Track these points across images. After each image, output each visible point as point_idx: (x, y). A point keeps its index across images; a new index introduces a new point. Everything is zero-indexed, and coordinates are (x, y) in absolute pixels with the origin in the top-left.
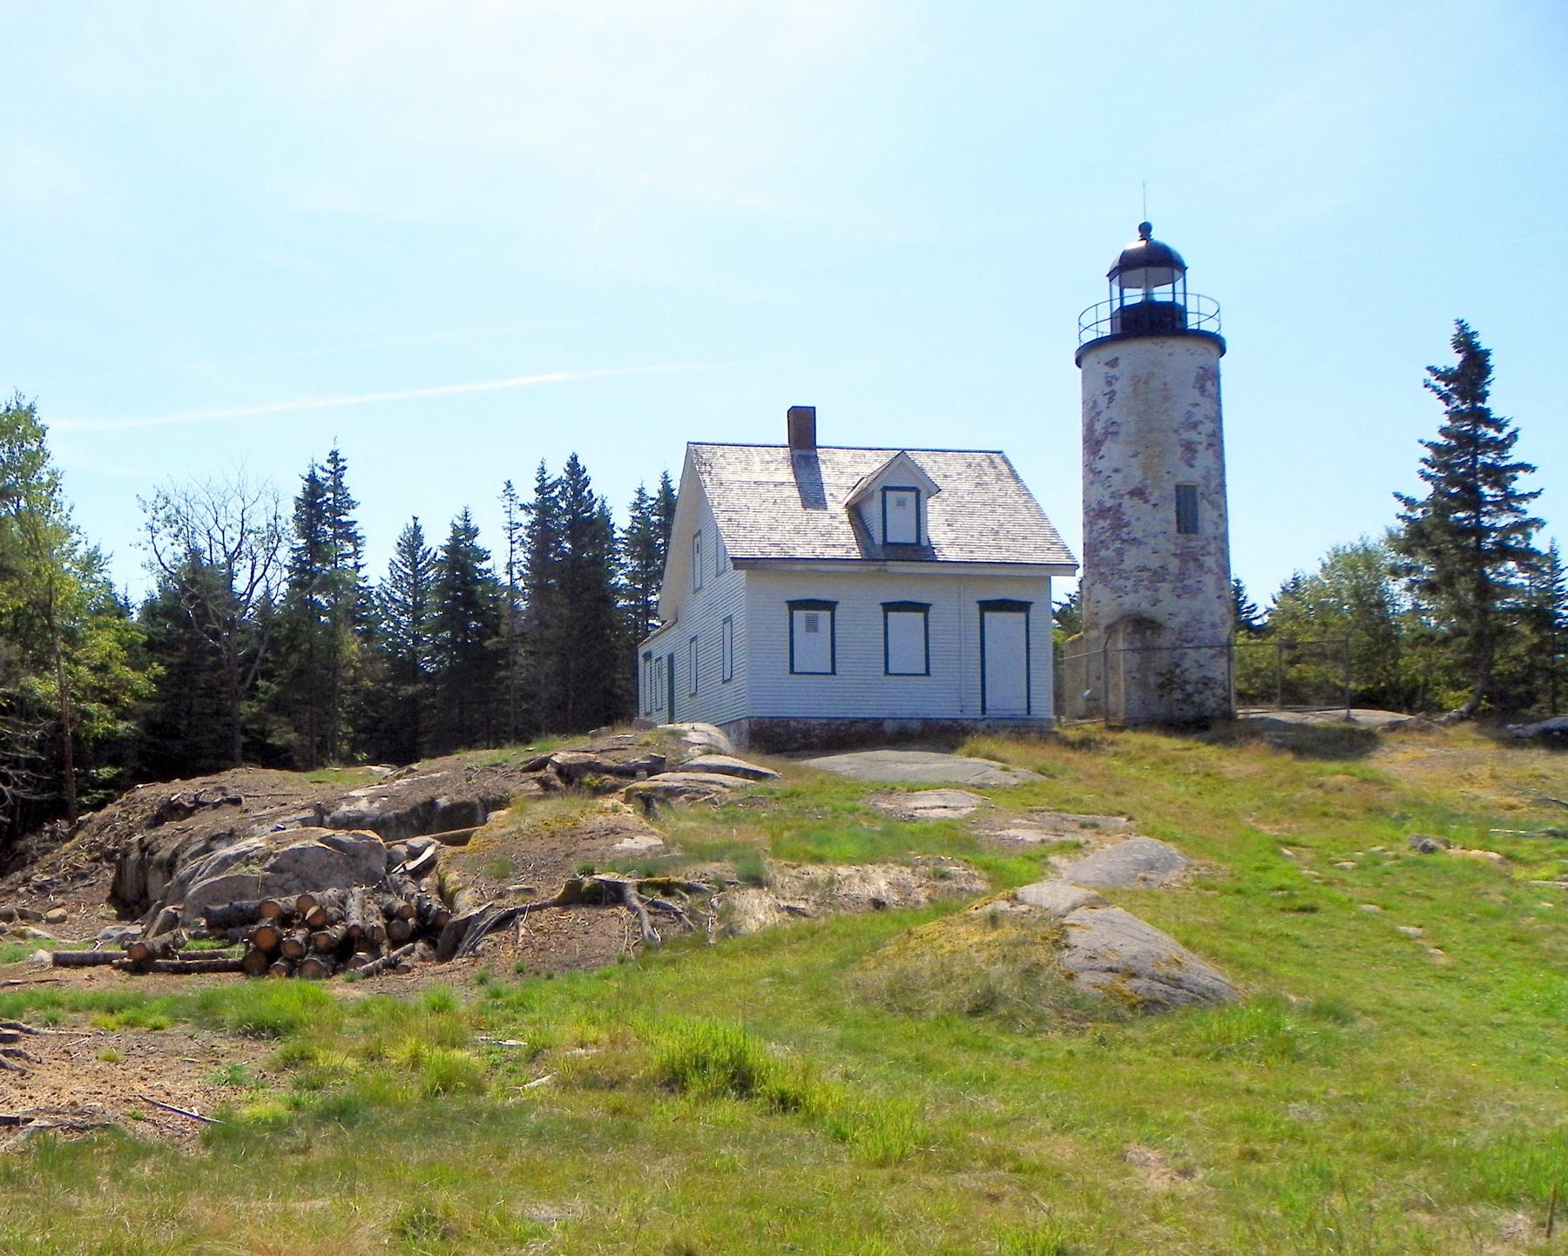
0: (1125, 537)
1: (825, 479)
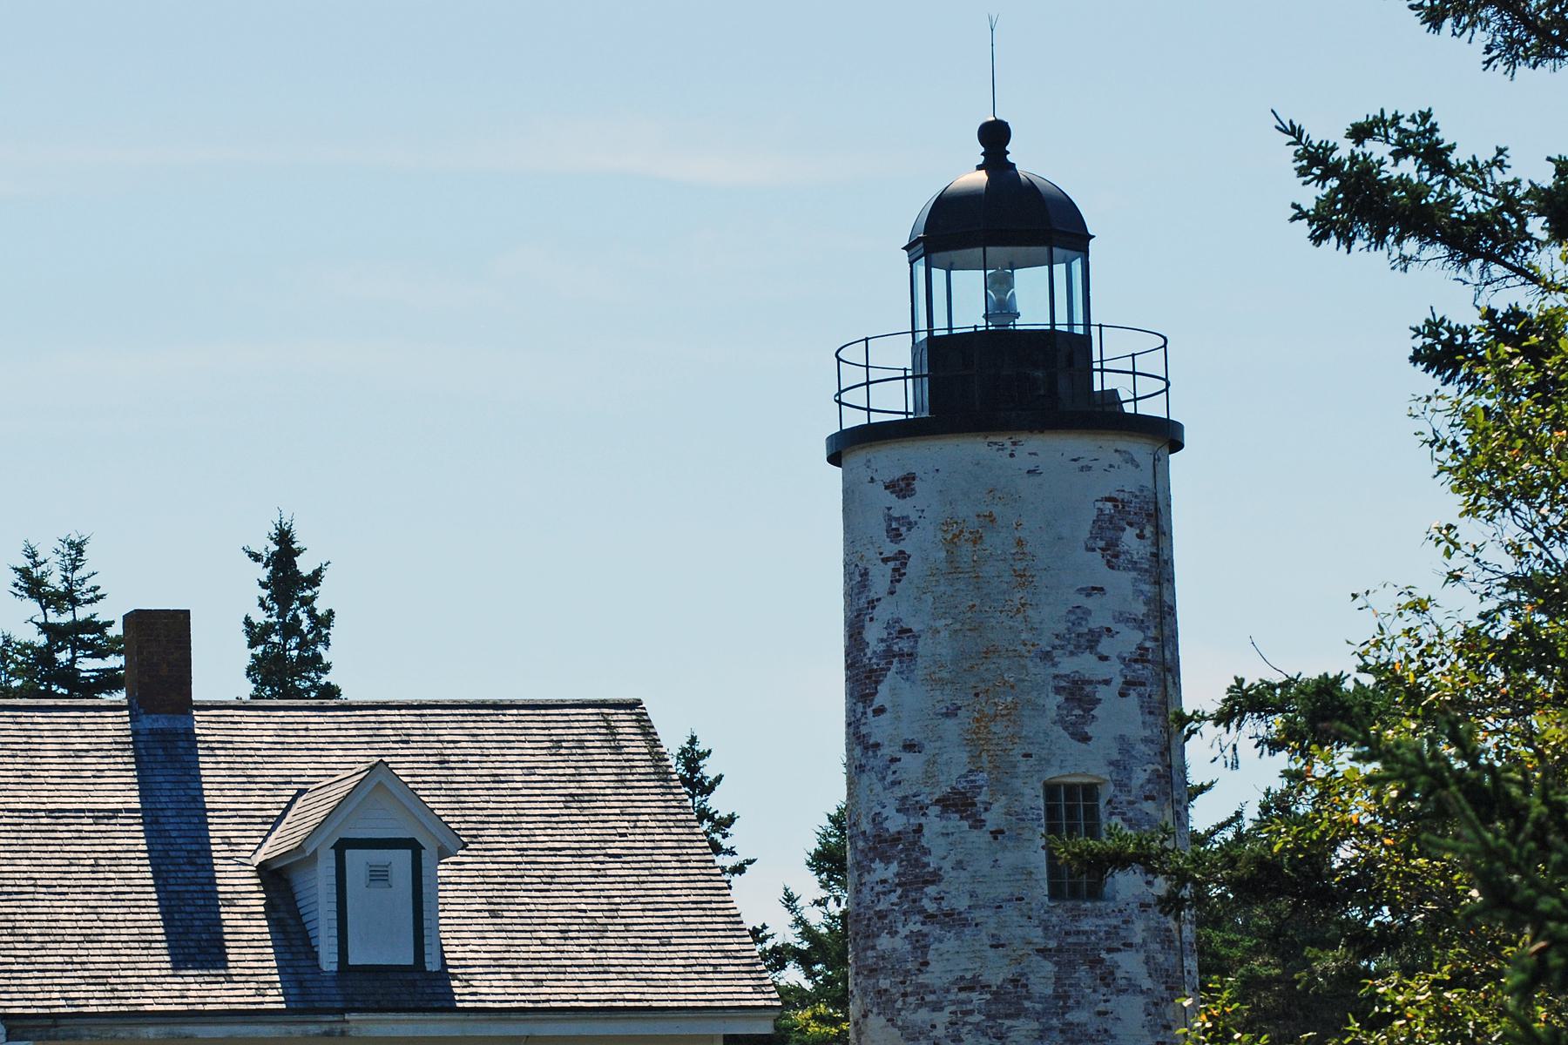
0: (931, 907)
1: (213, 798)
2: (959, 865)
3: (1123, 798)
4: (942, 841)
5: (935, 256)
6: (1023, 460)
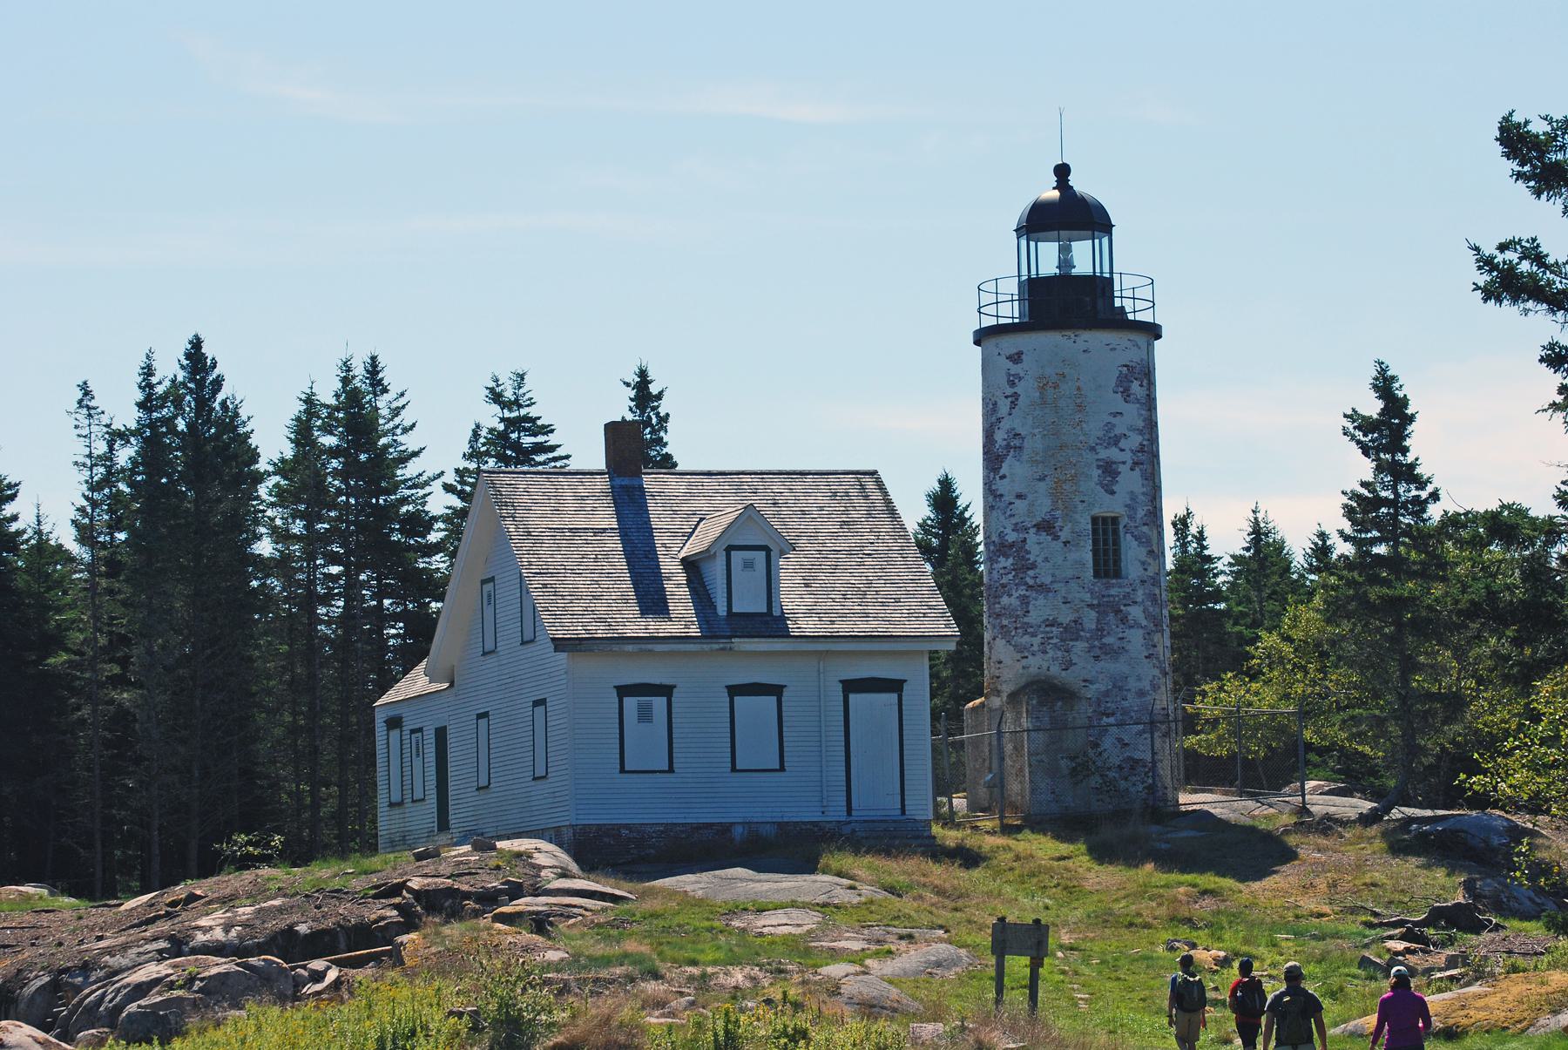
0: (1031, 582)
1: (655, 523)
2: (1046, 560)
6: (1081, 345)
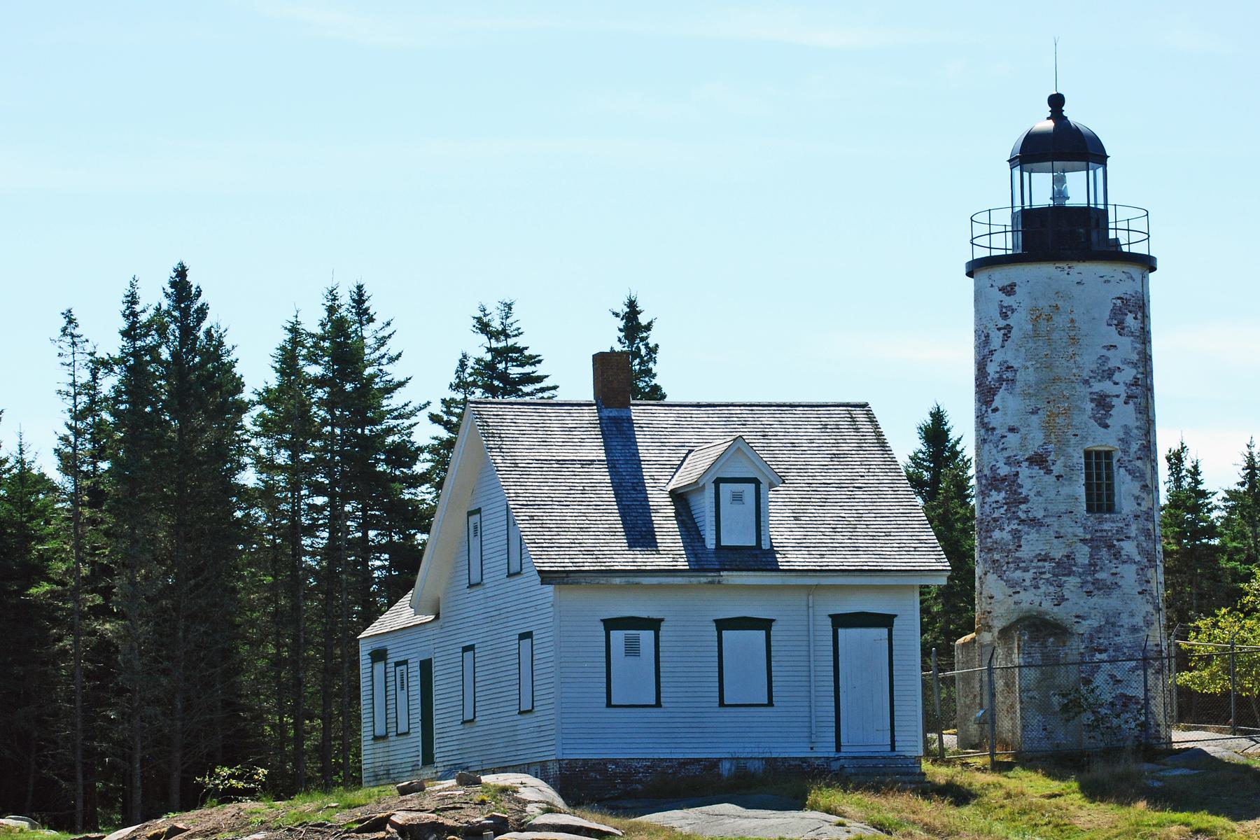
0: (1023, 516)
1: (643, 454)
2: (1039, 494)
3: (1126, 458)
4: (1029, 480)
5: (1026, 166)
